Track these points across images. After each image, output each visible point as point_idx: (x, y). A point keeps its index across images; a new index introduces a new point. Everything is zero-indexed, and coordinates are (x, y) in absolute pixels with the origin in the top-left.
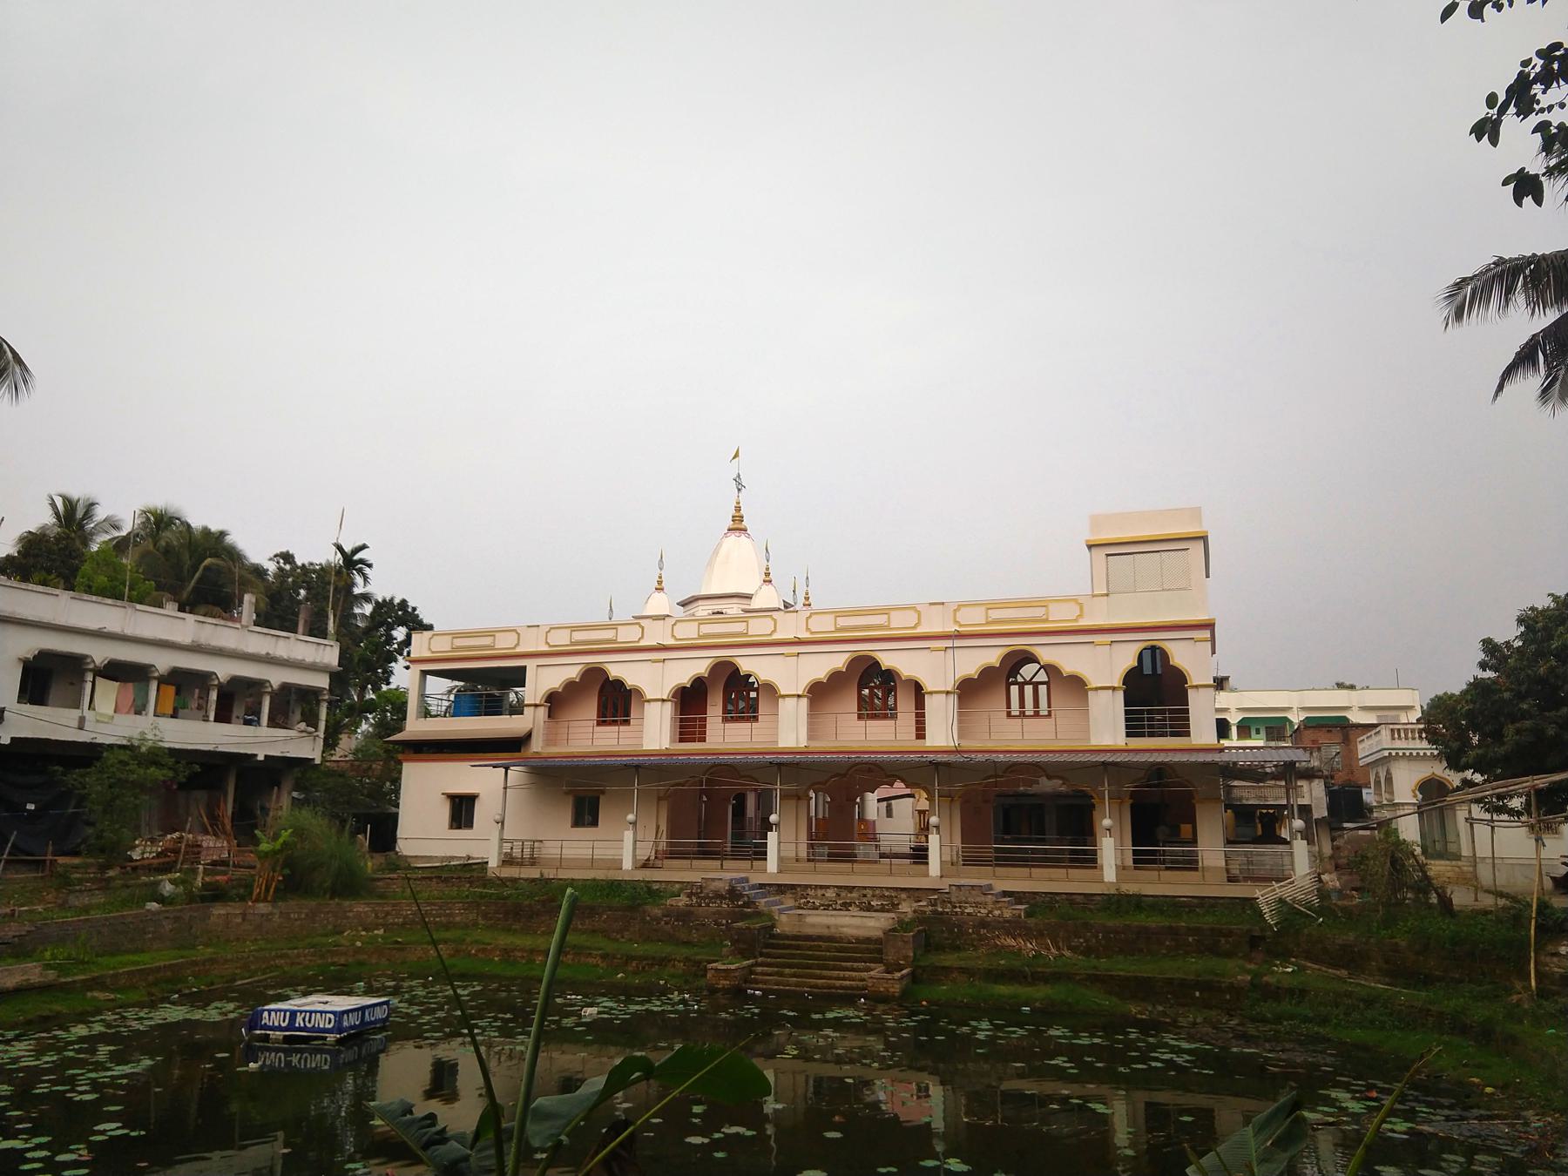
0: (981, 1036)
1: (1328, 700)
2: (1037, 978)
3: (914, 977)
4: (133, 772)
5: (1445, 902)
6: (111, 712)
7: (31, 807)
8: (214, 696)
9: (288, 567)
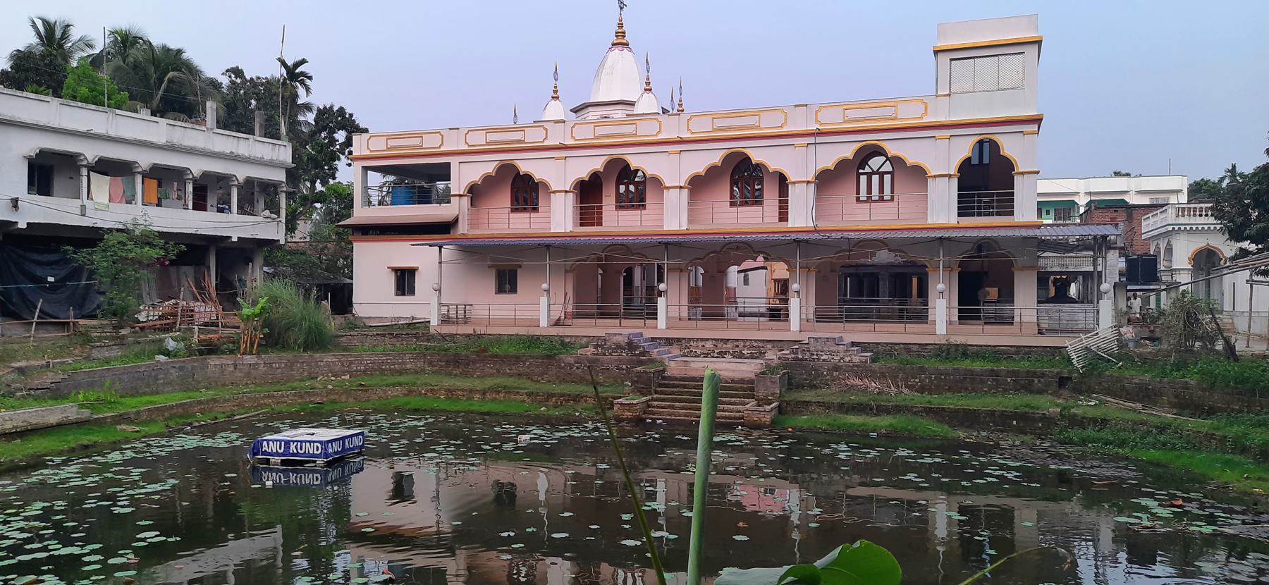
0: (842, 456)
1: (1109, 186)
2: (880, 410)
3: (780, 410)
4: (131, 251)
5: (1230, 348)
6: (107, 202)
7: (51, 279)
8: (190, 188)
9: (239, 81)
